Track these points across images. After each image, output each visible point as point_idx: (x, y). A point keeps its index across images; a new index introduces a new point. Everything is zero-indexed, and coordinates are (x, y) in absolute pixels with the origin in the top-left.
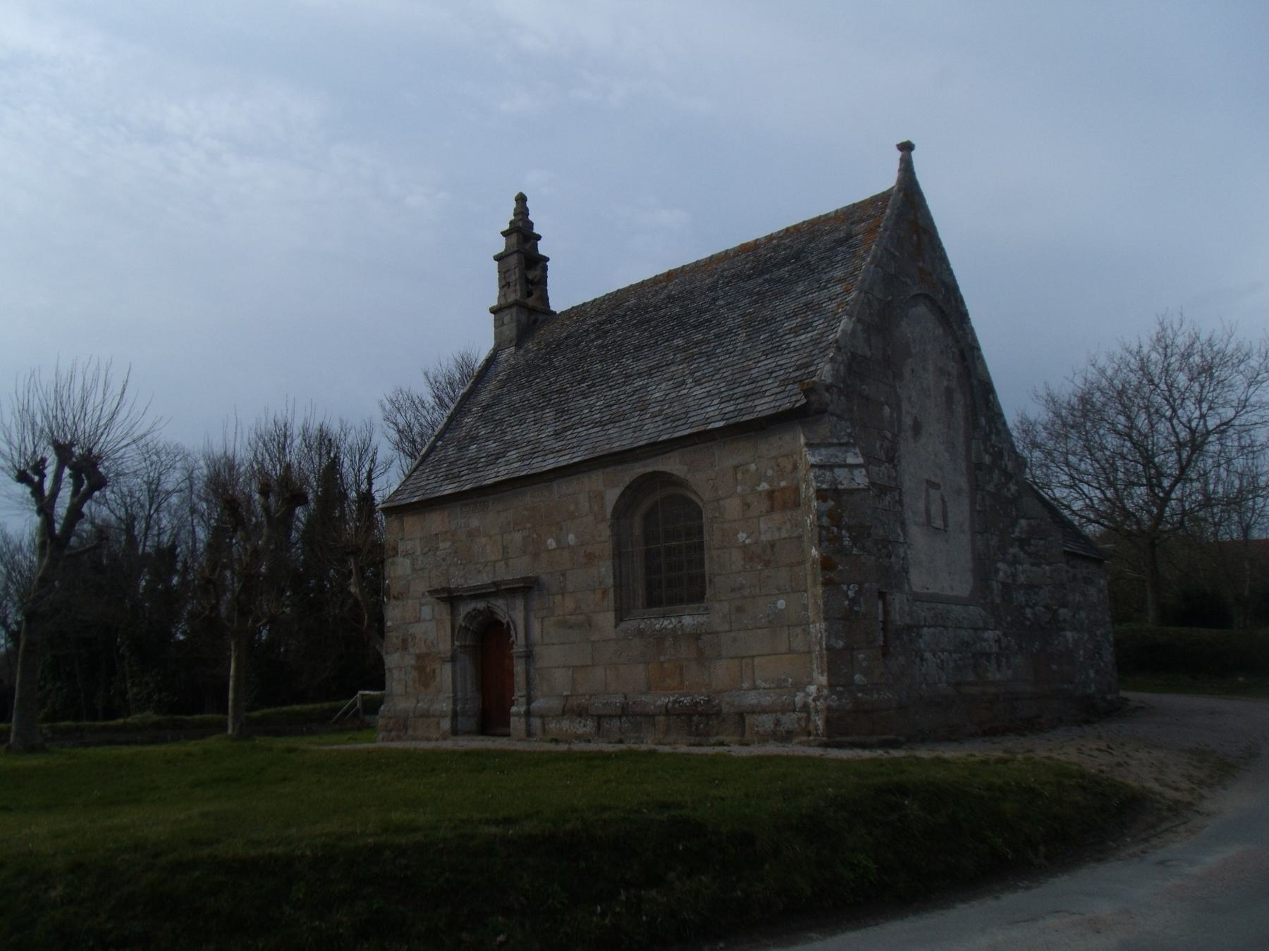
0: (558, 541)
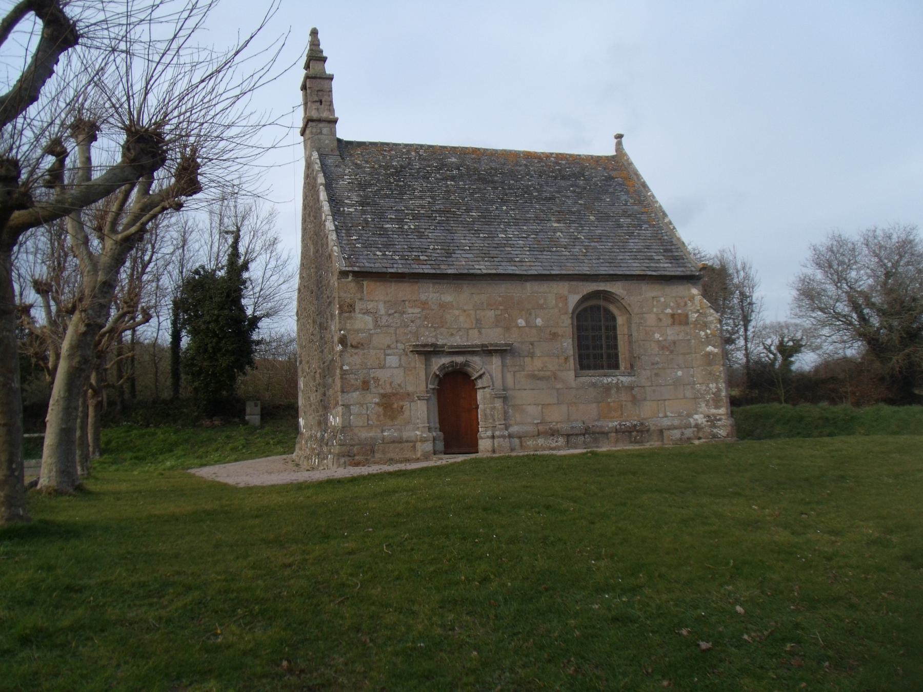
0: (527, 321)
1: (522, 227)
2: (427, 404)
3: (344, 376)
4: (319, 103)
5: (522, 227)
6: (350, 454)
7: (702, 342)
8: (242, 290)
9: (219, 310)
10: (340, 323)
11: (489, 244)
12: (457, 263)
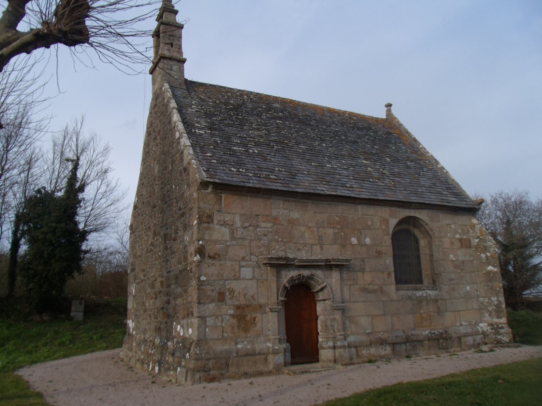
0: (359, 240)
1: (341, 161)
2: (278, 314)
3: (202, 287)
4: (170, 46)
5: (341, 161)
6: (205, 369)
7: (484, 262)
8: (77, 208)
9: (56, 223)
10: (199, 233)
11: (321, 171)
12: (302, 184)
